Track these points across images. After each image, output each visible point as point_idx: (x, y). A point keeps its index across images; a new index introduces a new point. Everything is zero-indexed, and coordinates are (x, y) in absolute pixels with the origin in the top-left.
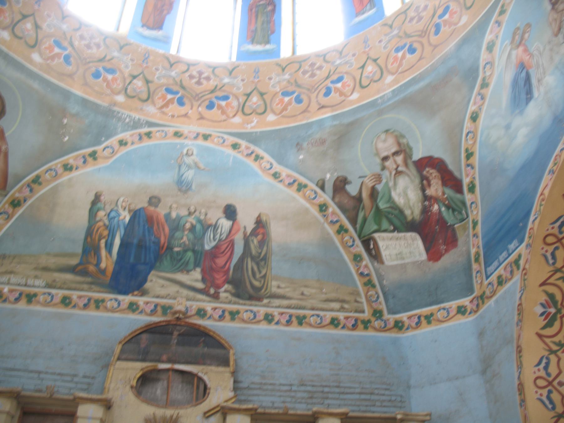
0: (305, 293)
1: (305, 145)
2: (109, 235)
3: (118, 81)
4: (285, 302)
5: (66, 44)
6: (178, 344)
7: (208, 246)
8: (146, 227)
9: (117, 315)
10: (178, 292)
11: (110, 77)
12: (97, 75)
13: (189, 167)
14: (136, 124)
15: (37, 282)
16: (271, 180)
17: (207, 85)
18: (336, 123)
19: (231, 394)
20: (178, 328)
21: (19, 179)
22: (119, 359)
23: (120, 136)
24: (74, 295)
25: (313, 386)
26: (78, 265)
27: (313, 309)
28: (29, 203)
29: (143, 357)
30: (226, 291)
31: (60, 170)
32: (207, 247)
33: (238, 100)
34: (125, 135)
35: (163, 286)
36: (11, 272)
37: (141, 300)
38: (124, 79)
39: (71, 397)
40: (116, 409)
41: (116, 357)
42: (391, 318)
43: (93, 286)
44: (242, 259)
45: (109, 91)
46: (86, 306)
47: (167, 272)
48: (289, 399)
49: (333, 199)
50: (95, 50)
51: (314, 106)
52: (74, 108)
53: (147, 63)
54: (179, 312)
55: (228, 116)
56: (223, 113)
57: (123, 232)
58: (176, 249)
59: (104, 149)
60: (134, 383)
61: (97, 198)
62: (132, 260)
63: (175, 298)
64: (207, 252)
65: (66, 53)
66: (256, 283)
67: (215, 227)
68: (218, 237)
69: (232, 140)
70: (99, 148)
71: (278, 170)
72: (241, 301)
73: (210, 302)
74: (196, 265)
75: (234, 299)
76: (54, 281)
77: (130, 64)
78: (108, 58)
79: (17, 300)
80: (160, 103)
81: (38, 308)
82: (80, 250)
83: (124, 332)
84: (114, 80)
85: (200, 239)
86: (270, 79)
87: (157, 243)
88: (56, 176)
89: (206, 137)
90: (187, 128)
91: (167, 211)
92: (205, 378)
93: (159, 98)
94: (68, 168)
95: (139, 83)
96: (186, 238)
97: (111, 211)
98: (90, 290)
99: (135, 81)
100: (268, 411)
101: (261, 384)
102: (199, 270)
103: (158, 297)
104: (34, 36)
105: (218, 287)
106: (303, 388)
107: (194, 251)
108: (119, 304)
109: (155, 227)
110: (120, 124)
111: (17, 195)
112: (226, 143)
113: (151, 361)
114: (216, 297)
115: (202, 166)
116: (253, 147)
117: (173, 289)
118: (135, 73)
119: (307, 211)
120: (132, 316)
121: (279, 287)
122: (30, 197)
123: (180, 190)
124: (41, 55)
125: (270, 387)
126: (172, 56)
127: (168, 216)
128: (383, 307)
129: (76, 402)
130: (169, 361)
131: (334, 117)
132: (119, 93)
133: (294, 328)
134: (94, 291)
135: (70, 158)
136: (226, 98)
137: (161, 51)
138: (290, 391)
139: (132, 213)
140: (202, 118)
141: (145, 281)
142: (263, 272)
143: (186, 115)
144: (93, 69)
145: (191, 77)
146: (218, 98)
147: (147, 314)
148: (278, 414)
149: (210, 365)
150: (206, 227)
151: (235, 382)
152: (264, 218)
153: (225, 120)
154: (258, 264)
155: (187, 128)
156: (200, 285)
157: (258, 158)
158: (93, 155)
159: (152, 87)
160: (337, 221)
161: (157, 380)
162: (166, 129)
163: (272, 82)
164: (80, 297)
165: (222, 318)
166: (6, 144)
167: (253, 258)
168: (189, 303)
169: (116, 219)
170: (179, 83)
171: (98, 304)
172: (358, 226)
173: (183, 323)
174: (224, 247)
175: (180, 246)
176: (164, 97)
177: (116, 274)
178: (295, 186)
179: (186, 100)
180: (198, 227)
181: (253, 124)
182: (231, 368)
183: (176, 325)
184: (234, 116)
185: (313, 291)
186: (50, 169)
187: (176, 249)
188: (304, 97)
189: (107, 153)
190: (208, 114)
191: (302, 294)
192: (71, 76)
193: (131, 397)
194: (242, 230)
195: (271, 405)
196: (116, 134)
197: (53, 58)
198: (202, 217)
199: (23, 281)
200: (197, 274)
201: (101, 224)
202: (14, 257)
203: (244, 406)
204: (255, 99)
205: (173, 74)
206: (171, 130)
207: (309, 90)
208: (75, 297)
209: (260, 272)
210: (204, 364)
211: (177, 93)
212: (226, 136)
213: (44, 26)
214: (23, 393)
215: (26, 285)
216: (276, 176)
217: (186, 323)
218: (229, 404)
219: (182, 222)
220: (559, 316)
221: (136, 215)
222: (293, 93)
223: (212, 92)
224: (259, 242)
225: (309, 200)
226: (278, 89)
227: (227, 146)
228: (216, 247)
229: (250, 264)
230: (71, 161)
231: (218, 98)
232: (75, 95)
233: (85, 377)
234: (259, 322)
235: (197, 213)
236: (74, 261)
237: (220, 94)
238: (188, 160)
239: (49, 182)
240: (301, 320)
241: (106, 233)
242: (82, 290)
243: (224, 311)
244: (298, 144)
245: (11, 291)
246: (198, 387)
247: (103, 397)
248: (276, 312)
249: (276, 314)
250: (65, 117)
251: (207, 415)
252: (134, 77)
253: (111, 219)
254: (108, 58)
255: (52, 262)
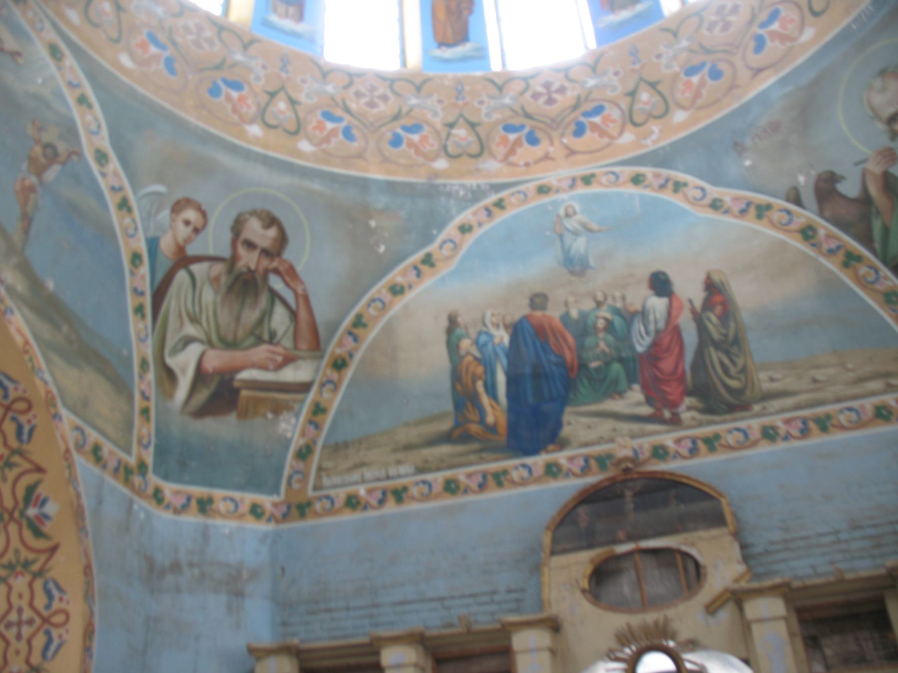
0: (820, 377)
1: (748, 142)
2: (485, 372)
3: (431, 141)
4: (790, 401)
5: (339, 112)
6: (637, 508)
7: (641, 347)
8: (538, 344)
9: (532, 488)
10: (615, 430)
11: (415, 138)
12: (396, 141)
13: (576, 233)
14: (477, 195)
15: (403, 470)
16: (710, 215)
17: (563, 101)
18: (789, 89)
19: (741, 568)
20: (630, 484)
21: (333, 328)
22: (553, 553)
23: (459, 220)
24: (461, 474)
25: (874, 526)
26: (452, 430)
27: (838, 400)
28: (358, 357)
29: (588, 541)
30: (689, 408)
31: (387, 297)
32: (640, 349)
33: (618, 106)
34: (466, 216)
35: (589, 427)
36: (363, 464)
37: (561, 457)
38: (437, 133)
39: (498, 626)
40: (567, 628)
41: (547, 551)
42: (154, 480)
43: (485, 455)
44: (700, 353)
45: (421, 160)
46: (482, 487)
47: (589, 403)
48: (839, 557)
49: (821, 214)
50: (382, 106)
51: (744, 74)
52: (380, 201)
53: (463, 98)
54: (626, 459)
55: (612, 138)
56: (602, 133)
57: (504, 360)
58: (594, 365)
59: (441, 247)
60: (585, 584)
61: (453, 322)
62: (531, 400)
63: (612, 441)
64: (641, 356)
65: (343, 124)
66: (734, 384)
67: (643, 313)
68: (652, 327)
69: (628, 171)
70: (432, 248)
71: (716, 196)
72: (716, 418)
73: (667, 432)
74: (631, 380)
75: (705, 417)
76: (426, 461)
77: (438, 108)
78: (405, 110)
79: (382, 502)
80: (501, 151)
81: (415, 506)
82: (449, 406)
83: (549, 510)
84: (424, 139)
85: (625, 339)
86: (659, 56)
87: (562, 364)
88: (385, 308)
89: (587, 180)
90: (555, 175)
91: (563, 309)
92: (693, 552)
93: (498, 145)
94: (397, 290)
95: (461, 132)
96: (603, 343)
97: (480, 334)
98: (482, 461)
99: (455, 131)
100: (809, 582)
101: (786, 541)
102: (636, 387)
103: (586, 445)
104: (293, 116)
105: (674, 405)
106: (857, 534)
107: (621, 360)
108: (333, 502)
109: (552, 340)
110: (452, 202)
111: (338, 351)
112: (621, 180)
113: (602, 544)
114: (675, 422)
115: (594, 226)
116: (665, 172)
117: (605, 427)
118: (451, 119)
119: (783, 245)
120: (554, 485)
121: (772, 380)
122: (357, 349)
123: (572, 273)
124: (310, 140)
125: (801, 543)
126: (497, 74)
127: (566, 318)
128: (149, 459)
129: (506, 630)
130: (631, 538)
131: (783, 82)
132: (435, 158)
133: (817, 439)
134: (488, 461)
135: (396, 276)
136: (598, 110)
137: (478, 74)
138: (839, 541)
139: (510, 330)
140: (572, 152)
141: (559, 425)
142: (740, 362)
143: (547, 157)
144: (389, 135)
145: (536, 96)
146: (586, 114)
147: (575, 475)
148: (829, 584)
149: (696, 529)
150: (629, 317)
151: (743, 547)
152: (716, 278)
153: (608, 145)
154: (727, 353)
155: (555, 175)
156: (646, 410)
157: (678, 186)
158: (428, 260)
159: (481, 131)
160: (839, 248)
161: (618, 572)
162: (522, 188)
163: (663, 60)
164: (469, 476)
165: (694, 451)
166: (302, 283)
167: (717, 345)
168: (636, 443)
169: (490, 346)
170: (520, 112)
171: (500, 479)
172: (877, 245)
173: (635, 476)
174: (666, 341)
175: (598, 359)
176: (505, 141)
177: (513, 428)
178: (752, 211)
179: (539, 134)
180: (617, 321)
181: (654, 137)
182: (731, 528)
183: (626, 480)
184: (621, 133)
185: (831, 371)
186: (373, 300)
187: (594, 365)
188: (723, 66)
189: (445, 252)
190: (577, 143)
191: (815, 381)
192: (360, 155)
193: (586, 607)
194: (687, 306)
195: (810, 571)
196: (451, 218)
197: (327, 139)
198: (619, 305)
199: (382, 473)
200: (636, 394)
201: (469, 358)
202: (360, 441)
203: (768, 583)
204: (645, 96)
205: (507, 101)
206: (531, 187)
207: (726, 51)
208: (462, 478)
209: (734, 363)
210: (685, 530)
211: (522, 127)
212: (617, 169)
213: (302, 98)
214: (429, 633)
215: (388, 478)
216: (716, 205)
217: (639, 473)
218: (743, 584)
219: (590, 322)
220: (21, 505)
221: (516, 330)
222: (703, 65)
223: (575, 107)
224: (719, 317)
225: (782, 227)
226: (677, 69)
227: (625, 183)
228: (655, 344)
229: (715, 356)
230: (400, 280)
231: (586, 114)
232: (375, 181)
233: (509, 591)
234: (755, 444)
235: (610, 301)
236: (446, 425)
237: (588, 107)
238: (571, 224)
239: (376, 319)
240: (824, 424)
241: (480, 370)
242: (470, 464)
243: (694, 442)
244: (736, 144)
245: (370, 492)
246: (685, 569)
247: (545, 614)
248: (778, 421)
249: (779, 424)
250: (370, 217)
251: (711, 609)
252: (451, 126)
253: (481, 347)
254: (405, 110)
255: (413, 434)
